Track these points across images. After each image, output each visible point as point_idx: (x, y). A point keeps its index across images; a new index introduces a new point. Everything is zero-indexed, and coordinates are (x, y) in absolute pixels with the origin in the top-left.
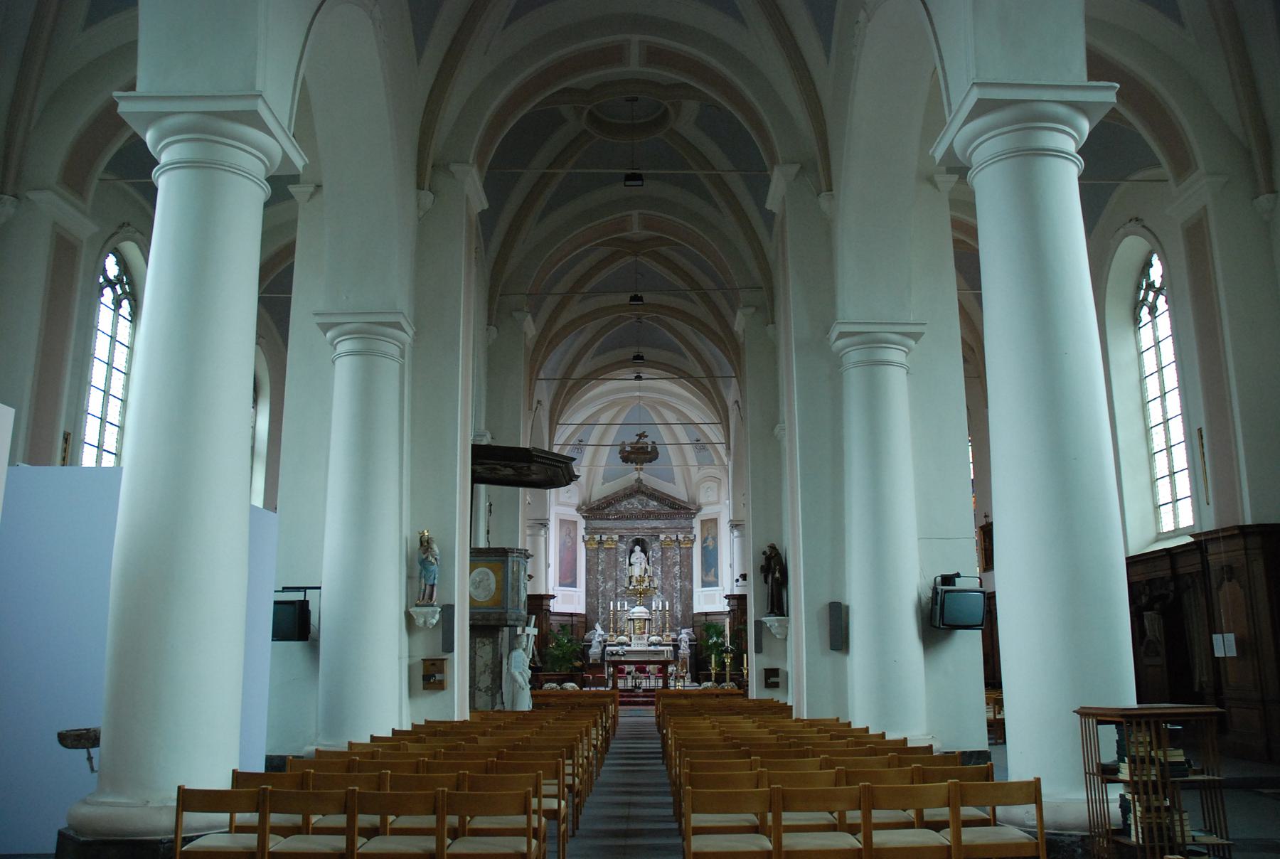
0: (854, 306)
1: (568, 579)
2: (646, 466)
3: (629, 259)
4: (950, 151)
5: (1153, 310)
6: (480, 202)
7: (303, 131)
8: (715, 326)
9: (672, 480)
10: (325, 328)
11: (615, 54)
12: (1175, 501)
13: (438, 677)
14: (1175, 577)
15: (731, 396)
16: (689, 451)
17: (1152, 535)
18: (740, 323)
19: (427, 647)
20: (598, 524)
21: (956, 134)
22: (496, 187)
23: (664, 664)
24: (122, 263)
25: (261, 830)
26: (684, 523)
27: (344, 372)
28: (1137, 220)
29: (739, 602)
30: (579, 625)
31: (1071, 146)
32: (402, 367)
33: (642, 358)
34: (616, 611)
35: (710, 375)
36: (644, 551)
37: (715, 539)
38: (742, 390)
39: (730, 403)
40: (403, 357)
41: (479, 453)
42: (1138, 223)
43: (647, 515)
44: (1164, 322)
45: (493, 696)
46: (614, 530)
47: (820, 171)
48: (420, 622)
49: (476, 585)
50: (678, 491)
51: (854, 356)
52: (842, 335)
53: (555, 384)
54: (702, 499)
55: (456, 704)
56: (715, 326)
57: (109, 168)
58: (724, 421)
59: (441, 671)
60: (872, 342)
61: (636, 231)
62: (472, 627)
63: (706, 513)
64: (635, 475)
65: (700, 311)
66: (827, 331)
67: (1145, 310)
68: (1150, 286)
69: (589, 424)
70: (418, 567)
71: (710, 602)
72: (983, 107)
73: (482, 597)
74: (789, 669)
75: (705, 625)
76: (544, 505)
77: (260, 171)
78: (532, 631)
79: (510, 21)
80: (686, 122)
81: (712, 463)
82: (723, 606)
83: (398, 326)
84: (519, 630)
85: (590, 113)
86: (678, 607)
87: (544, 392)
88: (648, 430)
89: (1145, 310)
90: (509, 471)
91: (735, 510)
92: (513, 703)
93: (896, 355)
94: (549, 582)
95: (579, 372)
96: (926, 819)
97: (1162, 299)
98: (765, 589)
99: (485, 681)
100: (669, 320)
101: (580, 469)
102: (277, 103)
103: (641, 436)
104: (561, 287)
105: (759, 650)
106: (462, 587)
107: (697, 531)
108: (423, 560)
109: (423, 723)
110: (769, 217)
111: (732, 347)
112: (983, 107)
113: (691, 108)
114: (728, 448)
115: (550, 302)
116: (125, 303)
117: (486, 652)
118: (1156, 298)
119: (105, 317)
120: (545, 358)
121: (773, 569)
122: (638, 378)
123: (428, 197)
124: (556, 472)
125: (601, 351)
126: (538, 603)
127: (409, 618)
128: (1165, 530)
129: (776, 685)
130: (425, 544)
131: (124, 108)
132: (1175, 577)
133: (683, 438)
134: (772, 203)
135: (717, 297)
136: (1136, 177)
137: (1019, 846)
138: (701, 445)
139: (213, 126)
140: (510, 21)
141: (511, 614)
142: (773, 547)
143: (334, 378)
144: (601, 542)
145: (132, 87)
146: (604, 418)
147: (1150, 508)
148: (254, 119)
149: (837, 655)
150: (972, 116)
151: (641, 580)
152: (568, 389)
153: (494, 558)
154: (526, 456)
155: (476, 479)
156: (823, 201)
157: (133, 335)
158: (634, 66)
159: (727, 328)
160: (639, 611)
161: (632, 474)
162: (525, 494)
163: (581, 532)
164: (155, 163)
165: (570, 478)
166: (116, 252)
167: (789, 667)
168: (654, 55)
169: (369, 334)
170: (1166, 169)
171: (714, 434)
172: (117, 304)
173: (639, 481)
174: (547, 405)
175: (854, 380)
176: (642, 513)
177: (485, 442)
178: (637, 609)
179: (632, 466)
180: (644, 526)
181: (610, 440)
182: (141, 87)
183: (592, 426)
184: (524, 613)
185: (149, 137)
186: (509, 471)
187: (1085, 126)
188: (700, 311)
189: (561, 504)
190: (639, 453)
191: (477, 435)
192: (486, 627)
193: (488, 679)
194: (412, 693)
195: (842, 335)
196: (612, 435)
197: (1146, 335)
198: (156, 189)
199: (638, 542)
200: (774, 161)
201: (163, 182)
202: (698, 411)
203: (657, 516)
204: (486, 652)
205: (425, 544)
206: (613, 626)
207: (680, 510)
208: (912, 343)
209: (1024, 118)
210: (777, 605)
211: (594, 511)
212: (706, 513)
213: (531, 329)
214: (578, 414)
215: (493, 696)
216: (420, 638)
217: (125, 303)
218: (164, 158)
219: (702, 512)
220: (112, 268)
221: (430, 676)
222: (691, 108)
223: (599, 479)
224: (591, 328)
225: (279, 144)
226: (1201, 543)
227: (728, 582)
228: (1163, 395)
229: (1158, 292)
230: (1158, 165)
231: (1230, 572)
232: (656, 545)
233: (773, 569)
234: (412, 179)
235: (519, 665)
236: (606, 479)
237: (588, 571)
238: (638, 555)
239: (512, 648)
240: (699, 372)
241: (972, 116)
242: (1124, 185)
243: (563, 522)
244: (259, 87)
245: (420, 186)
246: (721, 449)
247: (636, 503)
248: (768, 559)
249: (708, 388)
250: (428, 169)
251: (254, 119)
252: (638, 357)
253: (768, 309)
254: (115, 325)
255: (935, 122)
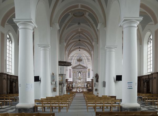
0: (108, 44)
1: (70, 77)
2: (81, 62)
3: (79, 34)
5: (150, 42)
6: (59, 28)
7: (37, 22)
8: (90, 43)
9: (84, 64)
10: (39, 46)
11: (77, 6)
13: (55, 90)
14: (149, 78)
15: (92, 53)
16: (86, 60)
17: (147, 72)
18: (93, 43)
19: (53, 87)
20: (74, 70)
21: (121, 23)
22: (60, 26)
23: (83, 88)
24: (9, 36)
26: (86, 69)
27: (42, 52)
29: (92, 80)
30: (72, 83)
31: (136, 25)
32: (49, 52)
33: (80, 40)
34: (76, 81)
35: (90, 50)
36: (80, 73)
37: (90, 72)
38: (93, 52)
39: (92, 54)
40: (49, 50)
41: (59, 62)
42: (149, 30)
43: (81, 69)
44: (151, 44)
45: (62, 92)
46: (76, 70)
47: (105, 24)
48: (53, 83)
49: (59, 79)
50: (85, 65)
51: (108, 50)
52: (106, 47)
53: (68, 51)
54: (88, 66)
55: (57, 94)
56: (90, 43)
57: (7, 22)
58: (91, 56)
59: (56, 89)
60: (110, 48)
61: (79, 31)
62: (59, 84)
63: (89, 68)
64: (79, 63)
65: (88, 41)
66: (104, 46)
67: (149, 42)
68: (150, 39)
69: (73, 57)
70: (52, 77)
71: (89, 80)
72: (125, 20)
73: (60, 80)
74: (98, 88)
75: (88, 83)
76: (67, 68)
77: (32, 29)
78: (66, 84)
79: (62, 2)
80: (87, 15)
81: (89, 62)
82: (91, 80)
83: (49, 46)
84: (65, 84)
85: (73, 14)
86: (85, 81)
87: (67, 53)
88: (81, 57)
89: (149, 42)
90: (63, 64)
91: (92, 68)
92: (64, 93)
93: (113, 50)
94: (67, 77)
95: (70, 42)
97: (152, 41)
98: (96, 79)
99: (61, 90)
100: (84, 43)
101: (72, 64)
102: (33, 20)
103: (80, 58)
104: (69, 39)
105: (95, 86)
106: (58, 79)
107: (87, 71)
108: (53, 75)
109: (55, 97)
110: (98, 30)
111: (92, 47)
112: (125, 20)
113: (87, 13)
114: (92, 60)
115: (67, 41)
116: (10, 41)
117: (61, 87)
118: (151, 41)
119: (8, 43)
120: (67, 48)
121: (97, 76)
122: (80, 50)
123: (52, 28)
124: (68, 64)
125: (74, 47)
126: (67, 80)
127: (51, 83)
129: (97, 91)
130: (53, 74)
131: (14, 21)
132: (149, 78)
133: (86, 58)
134: (98, 28)
135: (91, 40)
138: (88, 59)
139: (26, 23)
140: (62, 2)
141: (64, 82)
142: (97, 74)
143: (41, 52)
144: (74, 72)
146: (75, 56)
147: (147, 69)
148: (31, 22)
149: (104, 87)
151: (80, 77)
152: (70, 52)
153: (61, 75)
154: (65, 62)
155: (59, 65)
156: (105, 28)
157: (12, 46)
158: (80, 8)
159: (92, 44)
160: (80, 81)
161: (78, 63)
162: (65, 67)
163: (72, 71)
165: (71, 65)
166: (8, 34)
167: (98, 88)
168: (82, 6)
169: (45, 47)
170: (153, 23)
171: (90, 58)
172: (9, 41)
173: (80, 64)
174: (67, 54)
175: (107, 53)
176: (80, 68)
177: (59, 61)
178: (79, 81)
179: (79, 62)
180: (80, 70)
181: (75, 59)
183: (73, 57)
184: (65, 82)
185: (18, 24)
186: (63, 64)
187: (138, 22)
188: (88, 41)
189: (69, 68)
190: (80, 60)
191: (59, 59)
192: (60, 84)
193: (61, 91)
194: (52, 92)
195: (106, 47)
196: (76, 58)
197: (149, 46)
198: (19, 31)
199: (79, 72)
200: (99, 22)
201: (20, 31)
202: (88, 54)
203: (82, 69)
204: (61, 87)
205: (53, 74)
206: (76, 83)
207: (85, 68)
208: (116, 48)
209: (130, 21)
210: (97, 81)
211: (74, 68)
212: (89, 68)
213: (65, 44)
214: (71, 55)
215: (62, 92)
216: (53, 85)
217: (10, 41)
218: (20, 27)
219: (88, 68)
220: (8, 37)
221: (54, 90)
222: (87, 13)
223: (74, 63)
224: (73, 44)
225: (34, 25)
226: (152, 74)
227: (91, 78)
228: (150, 54)
229: (151, 40)
230: (152, 21)
231: (155, 78)
232: (82, 72)
233: (97, 76)
234: (50, 26)
235: (65, 88)
236: (75, 64)
237: (73, 76)
238: (79, 74)
239: (64, 86)
240: (88, 50)
243: (69, 69)
244: (31, 18)
245: (51, 26)
246: (91, 60)
247: (79, 67)
248: (96, 75)
249: (89, 52)
250: (51, 24)
251: (31, 22)
252: (80, 48)
253: (97, 42)
254: (9, 44)
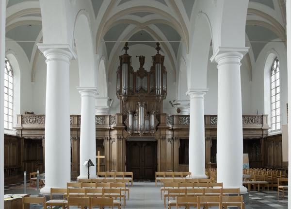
4: (214, 59)
12: (276, 123)
25: (185, 176)
28: (274, 49)
44: (278, 75)
96: (121, 131)
112: (220, 53)
116: (10, 72)
119: (6, 76)
128: (277, 129)
136: (274, 41)
137: (15, 55)
145: (79, 86)
150: (218, 54)
164: (46, 59)
182: (80, 86)
185: (44, 53)
197: (273, 77)
201: (48, 63)
241: (218, 54)
242: (269, 43)
255: (211, 53)
